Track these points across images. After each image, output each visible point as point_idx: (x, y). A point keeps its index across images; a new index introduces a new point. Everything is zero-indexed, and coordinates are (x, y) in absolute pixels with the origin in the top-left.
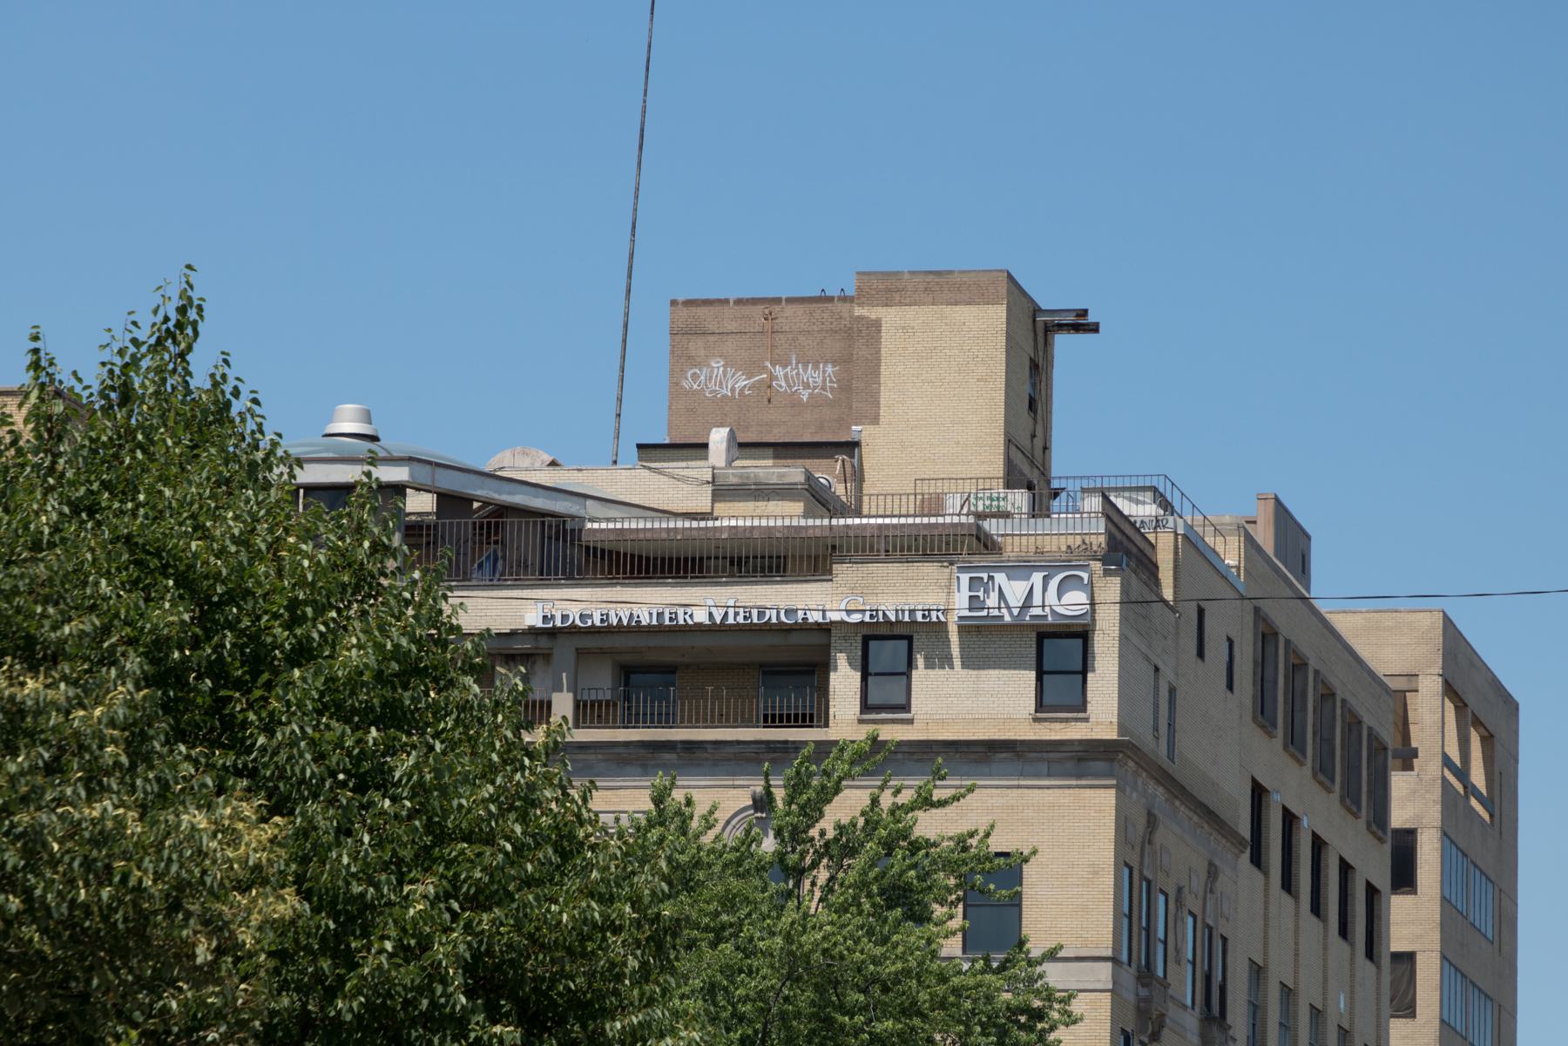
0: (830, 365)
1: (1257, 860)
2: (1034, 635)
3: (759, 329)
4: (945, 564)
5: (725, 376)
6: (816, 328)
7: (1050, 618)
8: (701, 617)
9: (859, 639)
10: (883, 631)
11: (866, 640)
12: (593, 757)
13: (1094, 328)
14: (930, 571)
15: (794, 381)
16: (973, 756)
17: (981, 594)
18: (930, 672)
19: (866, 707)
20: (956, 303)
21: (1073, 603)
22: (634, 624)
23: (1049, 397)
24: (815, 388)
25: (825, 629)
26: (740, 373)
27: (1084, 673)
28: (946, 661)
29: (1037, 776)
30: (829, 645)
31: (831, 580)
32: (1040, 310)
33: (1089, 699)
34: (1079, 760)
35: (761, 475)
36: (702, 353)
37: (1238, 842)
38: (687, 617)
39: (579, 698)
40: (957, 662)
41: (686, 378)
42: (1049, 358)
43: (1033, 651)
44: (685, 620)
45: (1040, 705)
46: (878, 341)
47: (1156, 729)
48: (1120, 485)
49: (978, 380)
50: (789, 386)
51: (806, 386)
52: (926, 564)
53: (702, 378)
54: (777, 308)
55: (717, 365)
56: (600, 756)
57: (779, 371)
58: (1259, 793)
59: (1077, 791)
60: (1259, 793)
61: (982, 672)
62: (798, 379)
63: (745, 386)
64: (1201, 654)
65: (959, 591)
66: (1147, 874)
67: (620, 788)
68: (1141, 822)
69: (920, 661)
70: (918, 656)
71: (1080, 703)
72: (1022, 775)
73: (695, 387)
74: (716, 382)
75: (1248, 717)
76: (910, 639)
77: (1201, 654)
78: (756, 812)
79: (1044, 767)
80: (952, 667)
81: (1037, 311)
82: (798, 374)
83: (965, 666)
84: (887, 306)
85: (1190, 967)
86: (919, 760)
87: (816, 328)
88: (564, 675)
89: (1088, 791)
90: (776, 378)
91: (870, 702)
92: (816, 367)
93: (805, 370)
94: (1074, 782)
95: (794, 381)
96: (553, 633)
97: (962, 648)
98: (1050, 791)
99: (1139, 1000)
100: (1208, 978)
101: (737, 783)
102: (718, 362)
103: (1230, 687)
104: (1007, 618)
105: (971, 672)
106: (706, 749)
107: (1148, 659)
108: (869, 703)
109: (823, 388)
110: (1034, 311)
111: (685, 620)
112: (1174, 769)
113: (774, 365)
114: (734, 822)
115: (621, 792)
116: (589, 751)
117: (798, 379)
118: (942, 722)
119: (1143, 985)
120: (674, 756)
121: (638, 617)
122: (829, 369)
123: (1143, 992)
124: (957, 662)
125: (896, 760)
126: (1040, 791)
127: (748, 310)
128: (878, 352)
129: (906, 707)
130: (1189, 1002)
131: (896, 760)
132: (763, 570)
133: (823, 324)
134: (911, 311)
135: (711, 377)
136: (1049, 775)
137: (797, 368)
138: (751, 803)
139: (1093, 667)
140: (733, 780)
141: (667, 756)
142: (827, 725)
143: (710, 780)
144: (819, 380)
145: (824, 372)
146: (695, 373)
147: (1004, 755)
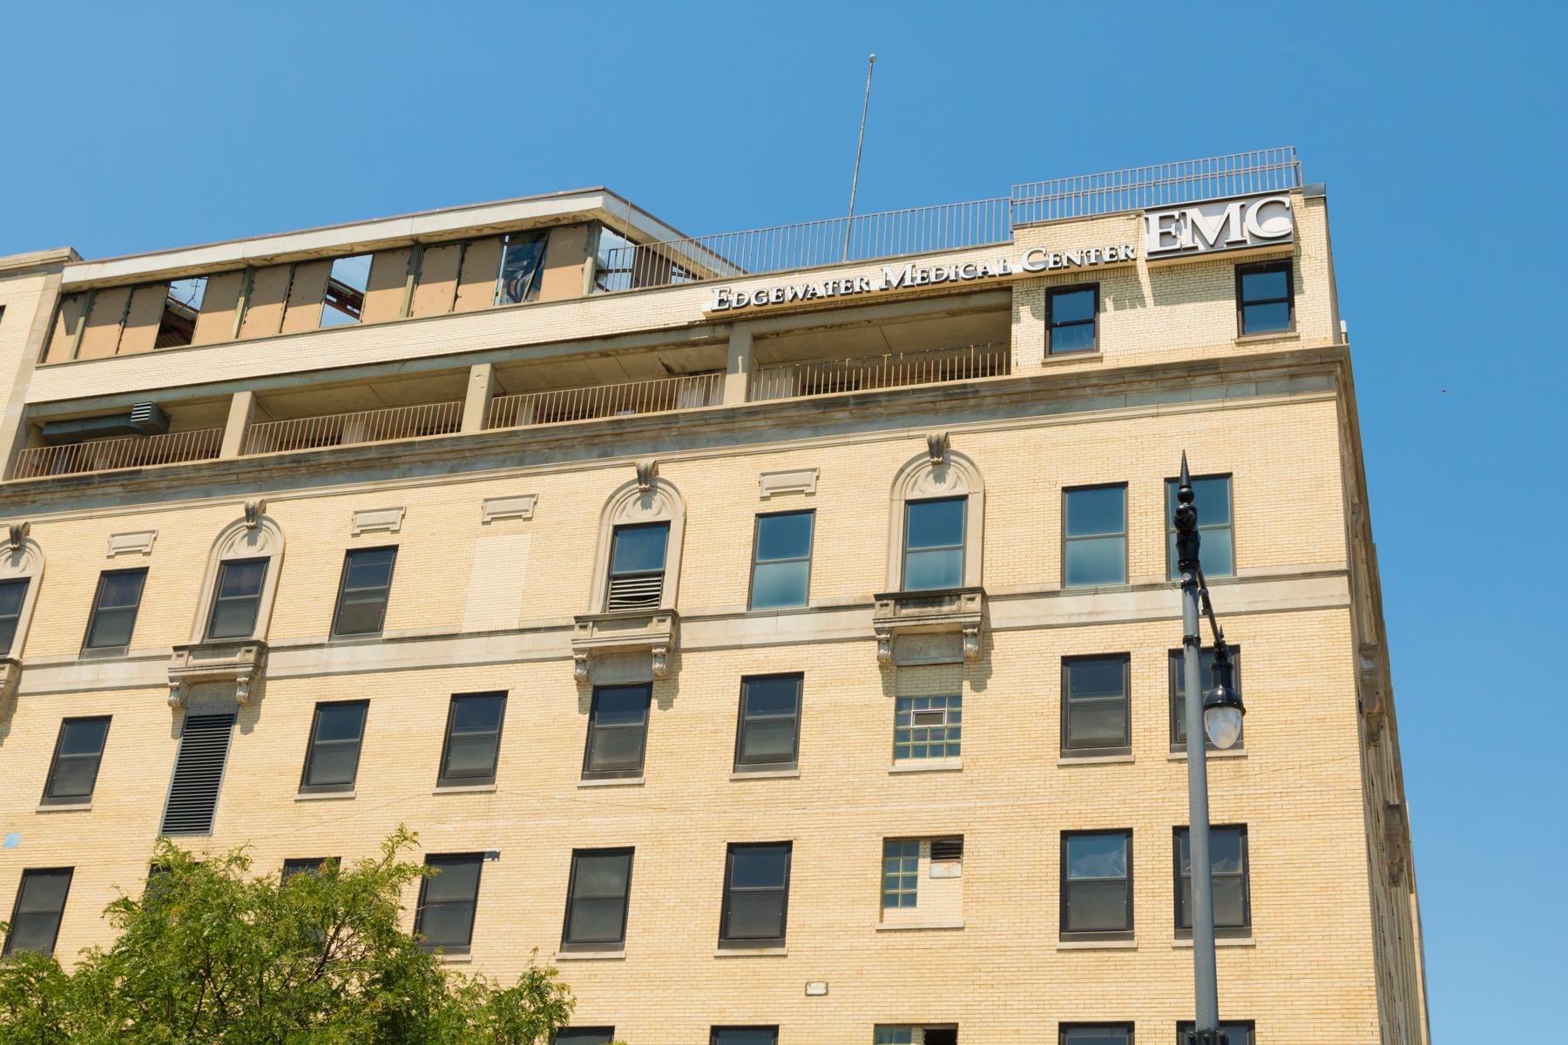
2: (1232, 268)
7: (1249, 242)
9: (1042, 292)
10: (1069, 281)
11: (1051, 293)
12: (763, 423)
16: (1169, 384)
17: (1172, 230)
18: (1119, 312)
21: (1277, 225)
27: (1290, 301)
28: (1139, 300)
29: (1244, 396)
30: (1008, 307)
31: (1012, 244)
34: (1292, 376)
40: (1149, 300)
43: (1232, 282)
44: (861, 287)
48: (1251, 373)
52: (1110, 219)
56: (770, 422)
59: (1292, 407)
61: (1176, 307)
65: (1148, 232)
67: (790, 450)
69: (1108, 303)
70: (1107, 300)
72: (1227, 396)
76: (1094, 288)
78: (932, 457)
79: (1252, 388)
80: (1144, 305)
83: (1157, 302)
86: (1110, 394)
88: (740, 358)
89: (1303, 406)
94: (1288, 399)
97: (1154, 288)
98: (1260, 410)
101: (911, 434)
104: (1202, 248)
105: (1164, 308)
106: (880, 401)
114: (908, 471)
115: (791, 454)
116: (758, 417)
119: (1366, 658)
120: (847, 414)
121: (814, 290)
124: (1149, 300)
125: (1086, 397)
126: (1249, 411)
131: (1086, 397)
136: (1258, 394)
138: (928, 449)
139: (1301, 288)
140: (908, 431)
141: (839, 415)
143: (884, 433)
147: (1206, 379)
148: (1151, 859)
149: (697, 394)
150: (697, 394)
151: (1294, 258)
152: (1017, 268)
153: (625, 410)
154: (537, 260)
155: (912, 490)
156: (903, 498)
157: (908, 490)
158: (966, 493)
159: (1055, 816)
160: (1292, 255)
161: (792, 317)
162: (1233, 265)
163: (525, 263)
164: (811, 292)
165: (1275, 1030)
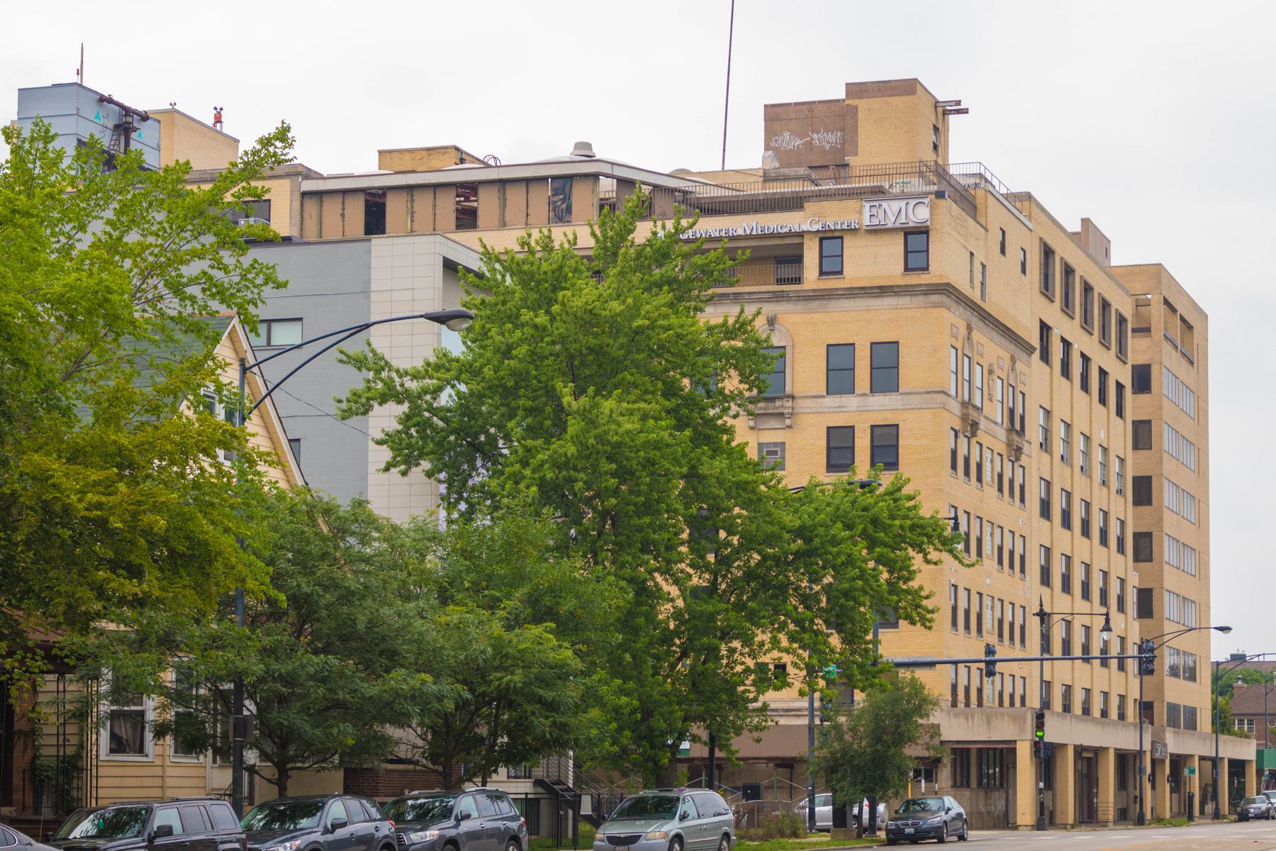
1: (1045, 357)
2: (902, 234)
8: (740, 232)
10: (830, 235)
11: (821, 240)
13: (966, 111)
14: (852, 204)
19: (822, 273)
23: (946, 146)
25: (801, 235)
37: (1029, 349)
43: (902, 241)
45: (907, 269)
46: (857, 115)
47: (971, 281)
51: (828, 142)
55: (786, 135)
57: (815, 136)
58: (1045, 328)
60: (1045, 328)
64: (1003, 251)
66: (967, 352)
68: (963, 331)
75: (1037, 291)
76: (842, 238)
77: (1003, 251)
81: (937, 102)
85: (954, 376)
92: (832, 134)
99: (963, 414)
100: (1012, 412)
103: (1024, 271)
107: (965, 247)
123: (965, 411)
129: (841, 272)
130: (999, 421)
134: (871, 101)
152: (805, 227)
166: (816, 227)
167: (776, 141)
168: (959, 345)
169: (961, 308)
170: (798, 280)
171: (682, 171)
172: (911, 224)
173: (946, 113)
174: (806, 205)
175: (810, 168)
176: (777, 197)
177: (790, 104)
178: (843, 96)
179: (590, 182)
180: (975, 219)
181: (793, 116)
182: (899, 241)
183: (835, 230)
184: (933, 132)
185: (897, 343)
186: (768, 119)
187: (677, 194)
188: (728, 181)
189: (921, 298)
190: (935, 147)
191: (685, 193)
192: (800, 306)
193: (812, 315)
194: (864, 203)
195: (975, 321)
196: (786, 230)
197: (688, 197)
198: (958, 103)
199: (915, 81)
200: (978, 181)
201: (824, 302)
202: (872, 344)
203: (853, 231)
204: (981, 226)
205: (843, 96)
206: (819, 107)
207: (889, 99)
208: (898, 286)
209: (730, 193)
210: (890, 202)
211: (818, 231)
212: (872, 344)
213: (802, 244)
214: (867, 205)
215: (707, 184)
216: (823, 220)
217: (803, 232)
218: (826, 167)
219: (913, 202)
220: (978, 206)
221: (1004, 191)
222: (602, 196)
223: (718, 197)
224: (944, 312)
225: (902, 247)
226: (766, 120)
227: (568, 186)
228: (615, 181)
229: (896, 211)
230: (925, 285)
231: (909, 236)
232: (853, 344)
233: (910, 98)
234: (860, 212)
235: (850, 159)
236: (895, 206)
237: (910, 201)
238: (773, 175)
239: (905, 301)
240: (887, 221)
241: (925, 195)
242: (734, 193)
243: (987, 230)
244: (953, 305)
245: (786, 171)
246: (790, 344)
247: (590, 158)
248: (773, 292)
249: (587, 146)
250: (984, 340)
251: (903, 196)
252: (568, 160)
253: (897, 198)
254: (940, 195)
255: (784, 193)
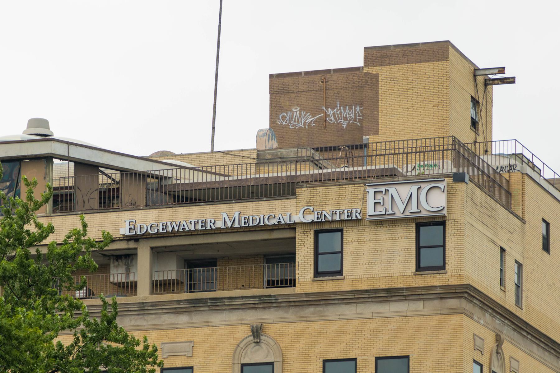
0: (358, 107)
3: (318, 88)
4: (362, 185)
5: (300, 116)
6: (350, 86)
8: (220, 224)
9: (312, 232)
10: (326, 227)
13: (511, 80)
14: (354, 190)
15: (338, 117)
19: (317, 273)
20: (420, 62)
22: (181, 230)
23: (489, 123)
24: (350, 120)
25: (292, 227)
26: (309, 114)
31: (295, 198)
32: (479, 69)
33: (446, 262)
35: (284, 153)
36: (288, 103)
38: (212, 224)
39: (153, 279)
41: (279, 119)
42: (489, 100)
43: (413, 235)
44: (210, 226)
45: (419, 268)
46: (377, 86)
49: (434, 106)
50: (336, 120)
51: (345, 119)
52: (350, 186)
53: (288, 118)
54: (328, 76)
55: (296, 110)
57: (330, 112)
62: (341, 115)
63: (311, 121)
64: (546, 247)
71: (442, 265)
73: (284, 123)
74: (295, 120)
76: (341, 231)
77: (546, 247)
81: (476, 69)
82: (340, 113)
84: (381, 66)
87: (350, 86)
90: (329, 116)
91: (320, 270)
92: (350, 108)
93: (345, 111)
95: (338, 117)
96: (136, 238)
102: (296, 109)
107: (493, 242)
108: (319, 271)
109: (355, 120)
110: (475, 70)
111: (210, 226)
112: (522, 314)
113: (327, 108)
117: (341, 115)
118: (361, 280)
122: (358, 109)
127: (312, 78)
128: (377, 92)
129: (340, 273)
132: (257, 196)
133: (354, 83)
134: (395, 68)
135: (292, 117)
137: (340, 109)
142: (295, 286)
144: (353, 115)
145: (355, 110)
146: (284, 116)
148: (381, 269)
149: (122, 270)
150: (122, 270)
151: (446, 221)
152: (298, 218)
153: (63, 194)
154: (16, 182)
155: (244, 358)
156: (240, 363)
157: (242, 358)
158: (273, 361)
159: (319, 194)
160: (445, 219)
161: (173, 237)
162: (415, 223)
163: (8, 184)
164: (182, 227)
165: (446, 350)
166: (311, 218)
167: (284, 118)
168: (484, 360)
169: (487, 315)
170: (291, 283)
171: (165, 154)
172: (424, 214)
173: (488, 83)
174: (299, 191)
175: (317, 150)
176: (269, 182)
177: (299, 74)
178: (359, 62)
179: (43, 164)
180: (508, 208)
181: (303, 87)
182: (410, 232)
183: (333, 222)
184: (470, 105)
185: (407, 357)
186: (273, 92)
187: (149, 180)
188: (201, 165)
189: (436, 302)
190: (474, 124)
191: (160, 178)
192: (291, 314)
193: (305, 325)
194: (368, 189)
195: (507, 332)
196: (274, 221)
197: (164, 183)
198: (502, 70)
199: (447, 44)
200: (513, 162)
201: (319, 309)
202: (377, 359)
203: (355, 222)
204: (517, 216)
205: (359, 62)
206: (335, 77)
207: (416, 66)
208: (407, 289)
209: (214, 178)
210: (399, 188)
211: (312, 223)
212: (377, 359)
213: (294, 238)
214: (371, 191)
215: (181, 167)
216: (320, 209)
217: (295, 223)
218: (336, 149)
219: (426, 187)
220: (514, 193)
221: (548, 175)
222: (56, 184)
223: (207, 183)
224: (464, 320)
225: (413, 242)
226: (271, 93)
227: (16, 171)
228: (72, 165)
229: (406, 198)
230: (441, 287)
231: (422, 229)
232: (355, 360)
233: (441, 64)
234: (364, 200)
235: (368, 138)
236: (405, 191)
237: (423, 185)
238: (268, 157)
239: (417, 306)
240: (395, 210)
241: (441, 178)
242: (222, 179)
243: (523, 221)
244: (477, 312)
245: (284, 152)
246: (280, 359)
247: (46, 138)
248: (259, 297)
249: (44, 123)
250: (519, 355)
251: (419, 180)
252: (19, 139)
253: (408, 181)
254: (458, 178)
255: (278, 177)
